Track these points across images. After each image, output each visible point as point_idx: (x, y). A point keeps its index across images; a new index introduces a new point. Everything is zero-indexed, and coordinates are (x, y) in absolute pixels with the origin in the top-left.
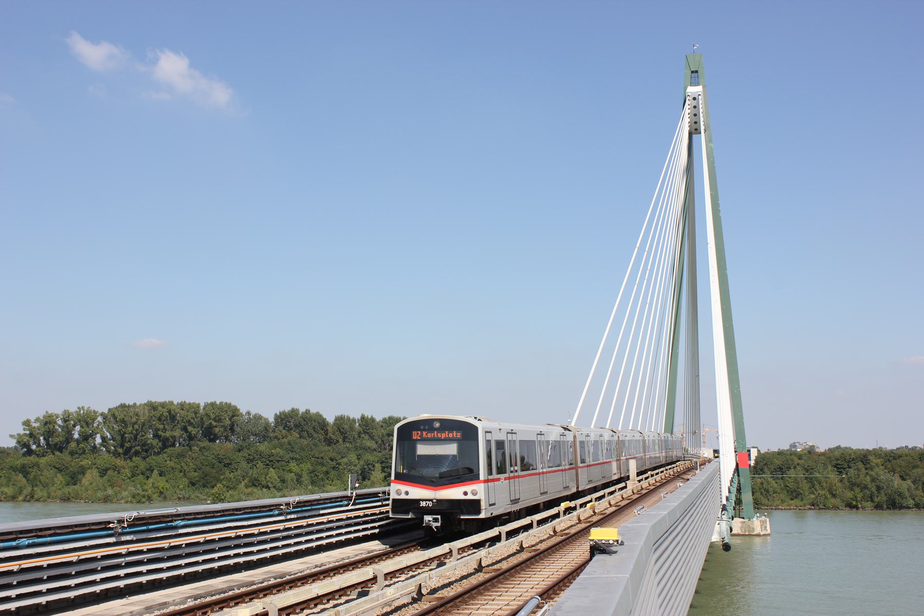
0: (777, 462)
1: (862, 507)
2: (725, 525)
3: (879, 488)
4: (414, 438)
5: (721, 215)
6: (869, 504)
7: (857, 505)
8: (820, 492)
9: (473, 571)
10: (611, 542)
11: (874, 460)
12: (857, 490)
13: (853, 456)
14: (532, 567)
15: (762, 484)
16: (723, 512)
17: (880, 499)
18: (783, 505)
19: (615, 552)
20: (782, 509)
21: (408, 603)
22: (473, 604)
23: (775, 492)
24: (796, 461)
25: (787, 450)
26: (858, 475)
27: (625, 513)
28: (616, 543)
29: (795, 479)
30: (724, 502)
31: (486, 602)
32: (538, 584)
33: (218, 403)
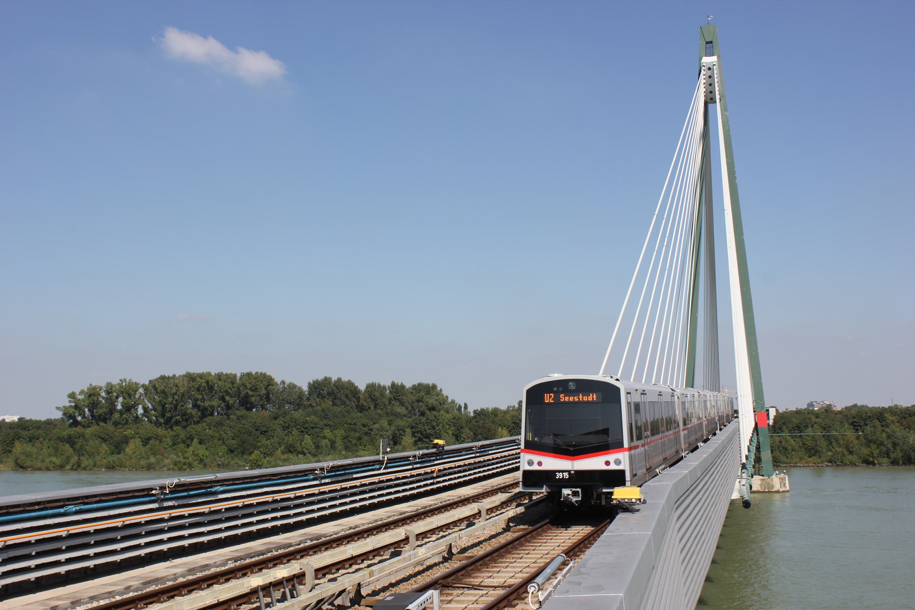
0: (796, 421)
3: (895, 445)
4: (546, 401)
6: (885, 460)
8: (837, 449)
10: (634, 501)
12: (874, 446)
15: (781, 442)
16: (743, 471)
19: (638, 510)
20: (800, 466)
21: (439, 562)
22: (502, 563)
24: (814, 419)
25: (805, 409)
28: (638, 502)
29: (813, 437)
30: (744, 461)
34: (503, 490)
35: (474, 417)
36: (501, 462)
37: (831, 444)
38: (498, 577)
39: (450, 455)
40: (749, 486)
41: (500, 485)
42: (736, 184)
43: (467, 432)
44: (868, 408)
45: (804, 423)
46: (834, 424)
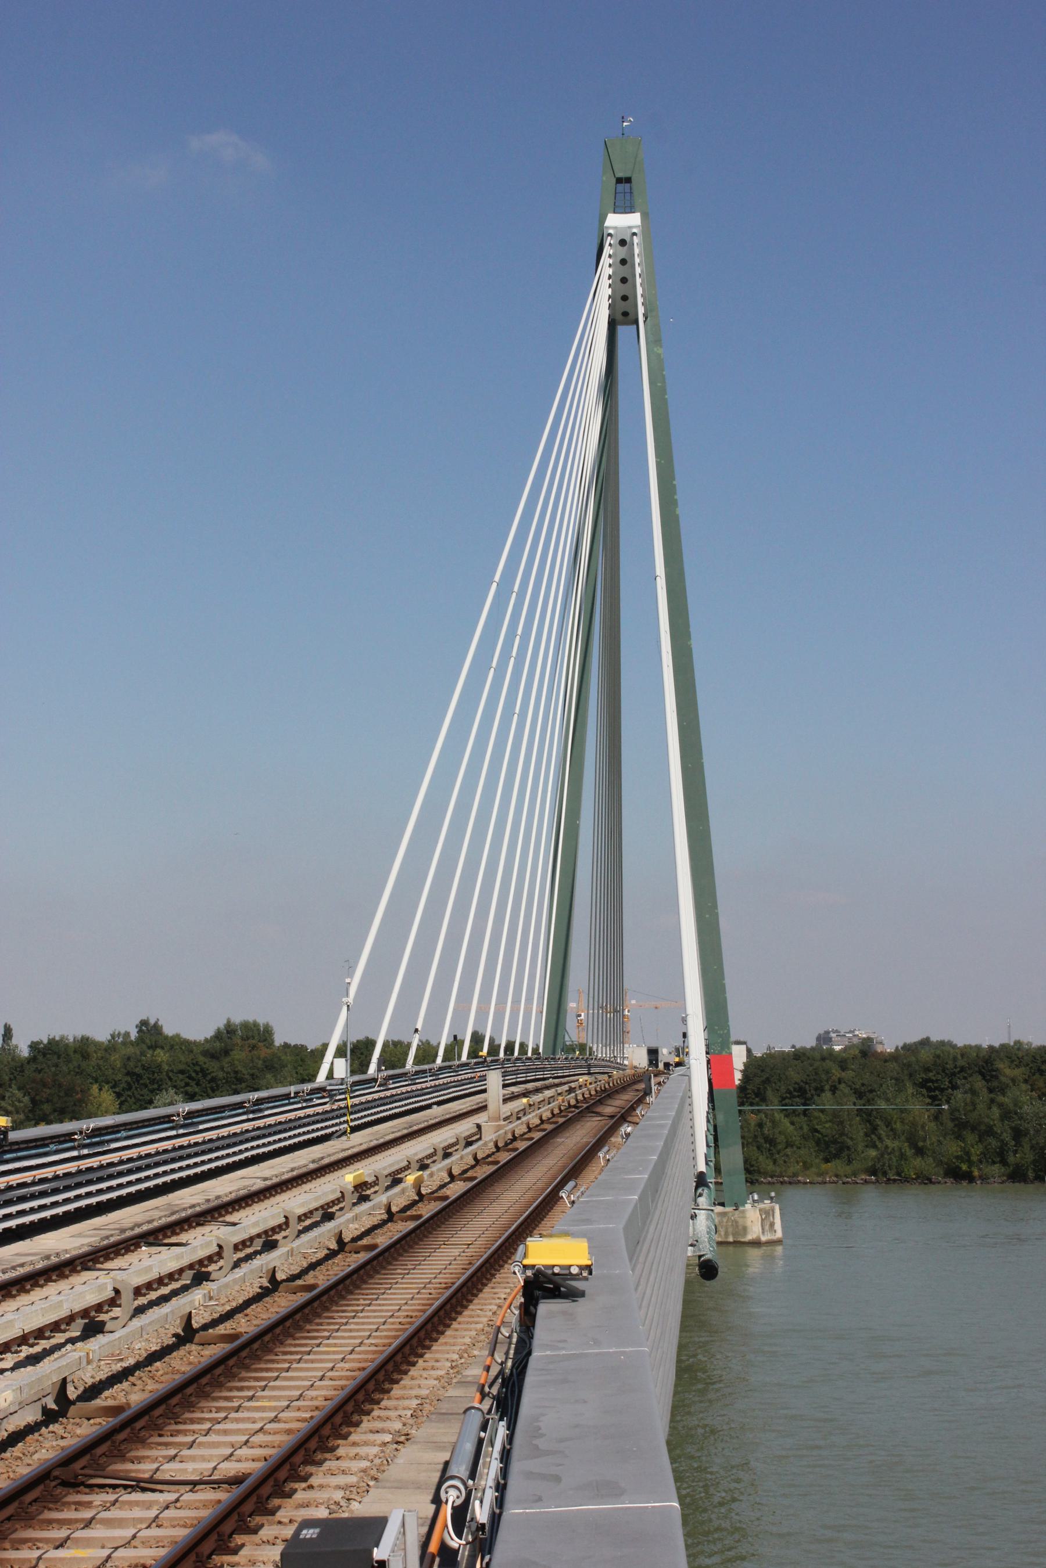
0: (795, 1075)
1: (981, 1177)
2: (704, 1221)
3: (1018, 1134)
5: (678, 511)
6: (996, 1169)
7: (971, 1172)
8: (888, 1142)
9: (172, 1341)
10: (575, 1270)
11: (1007, 1071)
12: (971, 1138)
13: (961, 1062)
14: (308, 1327)
15: (760, 1125)
16: (700, 1191)
17: (1022, 1158)
18: (808, 1172)
19: (582, 1294)
20: (806, 1183)
21: (36, 1423)
22: (192, 1421)
23: (789, 1144)
24: (837, 1073)
25: (812, 1049)
26: (974, 1104)
27: (493, 1196)
28: (585, 1274)
29: (835, 1114)
30: (702, 1167)
31: (222, 1415)
32: (332, 1369)
33: (946, 1041)
34: (151, 1239)
35: (32, 1060)
36: (139, 1169)
37: (874, 1129)
38: (193, 1459)
39: (20, 1154)
40: (713, 1227)
41: (139, 1225)
42: (678, 515)
43: (13, 1095)
44: (954, 1047)
45: (815, 1080)
46: (881, 1085)
